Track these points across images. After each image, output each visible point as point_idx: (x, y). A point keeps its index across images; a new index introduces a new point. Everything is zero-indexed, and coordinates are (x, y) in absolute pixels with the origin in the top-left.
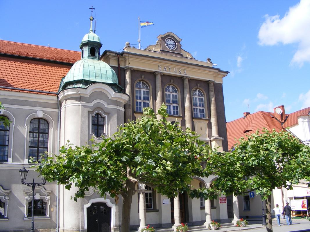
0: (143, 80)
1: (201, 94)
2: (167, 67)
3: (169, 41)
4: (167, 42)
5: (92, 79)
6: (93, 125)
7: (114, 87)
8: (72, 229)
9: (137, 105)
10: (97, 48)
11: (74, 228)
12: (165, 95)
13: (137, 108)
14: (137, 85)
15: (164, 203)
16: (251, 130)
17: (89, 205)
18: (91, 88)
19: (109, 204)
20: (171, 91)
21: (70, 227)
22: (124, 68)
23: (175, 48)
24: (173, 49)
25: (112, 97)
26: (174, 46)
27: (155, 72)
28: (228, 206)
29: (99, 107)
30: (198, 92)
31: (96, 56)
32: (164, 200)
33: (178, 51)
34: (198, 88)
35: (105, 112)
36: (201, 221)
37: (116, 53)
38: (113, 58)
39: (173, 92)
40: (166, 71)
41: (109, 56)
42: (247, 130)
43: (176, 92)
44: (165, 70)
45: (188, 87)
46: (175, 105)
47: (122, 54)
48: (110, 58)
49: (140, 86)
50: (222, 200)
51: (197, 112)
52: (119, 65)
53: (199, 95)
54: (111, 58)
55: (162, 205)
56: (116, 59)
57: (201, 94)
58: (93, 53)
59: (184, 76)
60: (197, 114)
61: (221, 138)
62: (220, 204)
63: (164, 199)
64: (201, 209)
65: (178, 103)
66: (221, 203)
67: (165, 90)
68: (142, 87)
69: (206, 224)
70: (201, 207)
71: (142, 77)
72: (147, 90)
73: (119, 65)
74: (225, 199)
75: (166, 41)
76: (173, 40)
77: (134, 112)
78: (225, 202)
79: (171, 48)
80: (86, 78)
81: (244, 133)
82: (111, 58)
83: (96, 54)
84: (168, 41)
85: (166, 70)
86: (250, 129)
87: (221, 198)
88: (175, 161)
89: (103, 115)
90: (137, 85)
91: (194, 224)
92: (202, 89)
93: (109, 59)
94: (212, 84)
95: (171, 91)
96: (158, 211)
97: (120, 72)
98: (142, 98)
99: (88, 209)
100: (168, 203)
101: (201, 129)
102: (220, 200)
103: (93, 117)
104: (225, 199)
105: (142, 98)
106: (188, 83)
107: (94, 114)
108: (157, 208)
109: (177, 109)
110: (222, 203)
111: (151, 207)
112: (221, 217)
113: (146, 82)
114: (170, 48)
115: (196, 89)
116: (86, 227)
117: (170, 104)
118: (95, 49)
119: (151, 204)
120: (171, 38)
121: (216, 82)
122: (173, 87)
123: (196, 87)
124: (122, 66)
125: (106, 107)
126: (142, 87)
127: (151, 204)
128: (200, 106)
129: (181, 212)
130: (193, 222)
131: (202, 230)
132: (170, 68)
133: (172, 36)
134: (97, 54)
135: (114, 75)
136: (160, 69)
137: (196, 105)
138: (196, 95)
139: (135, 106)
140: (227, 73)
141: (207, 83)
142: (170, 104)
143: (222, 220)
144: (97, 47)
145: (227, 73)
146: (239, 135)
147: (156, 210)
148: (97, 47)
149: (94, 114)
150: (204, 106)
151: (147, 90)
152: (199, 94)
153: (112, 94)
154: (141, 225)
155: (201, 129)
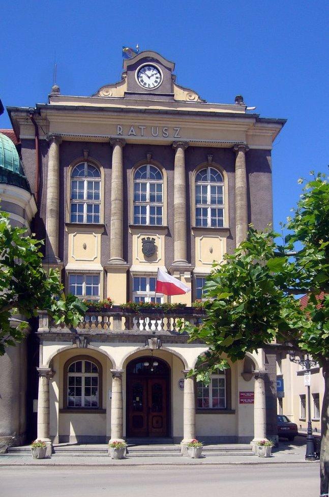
0: (87, 161)
2: (133, 126)
26: (156, 82)
37: (27, 111)
38: (26, 123)
44: (130, 133)
46: (156, 204)
47: (39, 111)
48: (20, 123)
49: (83, 172)
66: (241, 402)
69: (254, 444)
71: (83, 155)
79: (149, 85)
82: (23, 123)
85: (134, 133)
87: (243, 392)
88: (295, 330)
92: (218, 166)
102: (241, 396)
110: (245, 403)
112: (239, 432)
113: (93, 163)
114: (147, 86)
117: (144, 204)
121: (251, 147)
123: (205, 163)
124: (24, 135)
126: (86, 173)
131: (158, 456)
132: (142, 127)
136: (121, 132)
140: (282, 123)
145: (282, 123)
147: (231, 410)
154: (184, 436)
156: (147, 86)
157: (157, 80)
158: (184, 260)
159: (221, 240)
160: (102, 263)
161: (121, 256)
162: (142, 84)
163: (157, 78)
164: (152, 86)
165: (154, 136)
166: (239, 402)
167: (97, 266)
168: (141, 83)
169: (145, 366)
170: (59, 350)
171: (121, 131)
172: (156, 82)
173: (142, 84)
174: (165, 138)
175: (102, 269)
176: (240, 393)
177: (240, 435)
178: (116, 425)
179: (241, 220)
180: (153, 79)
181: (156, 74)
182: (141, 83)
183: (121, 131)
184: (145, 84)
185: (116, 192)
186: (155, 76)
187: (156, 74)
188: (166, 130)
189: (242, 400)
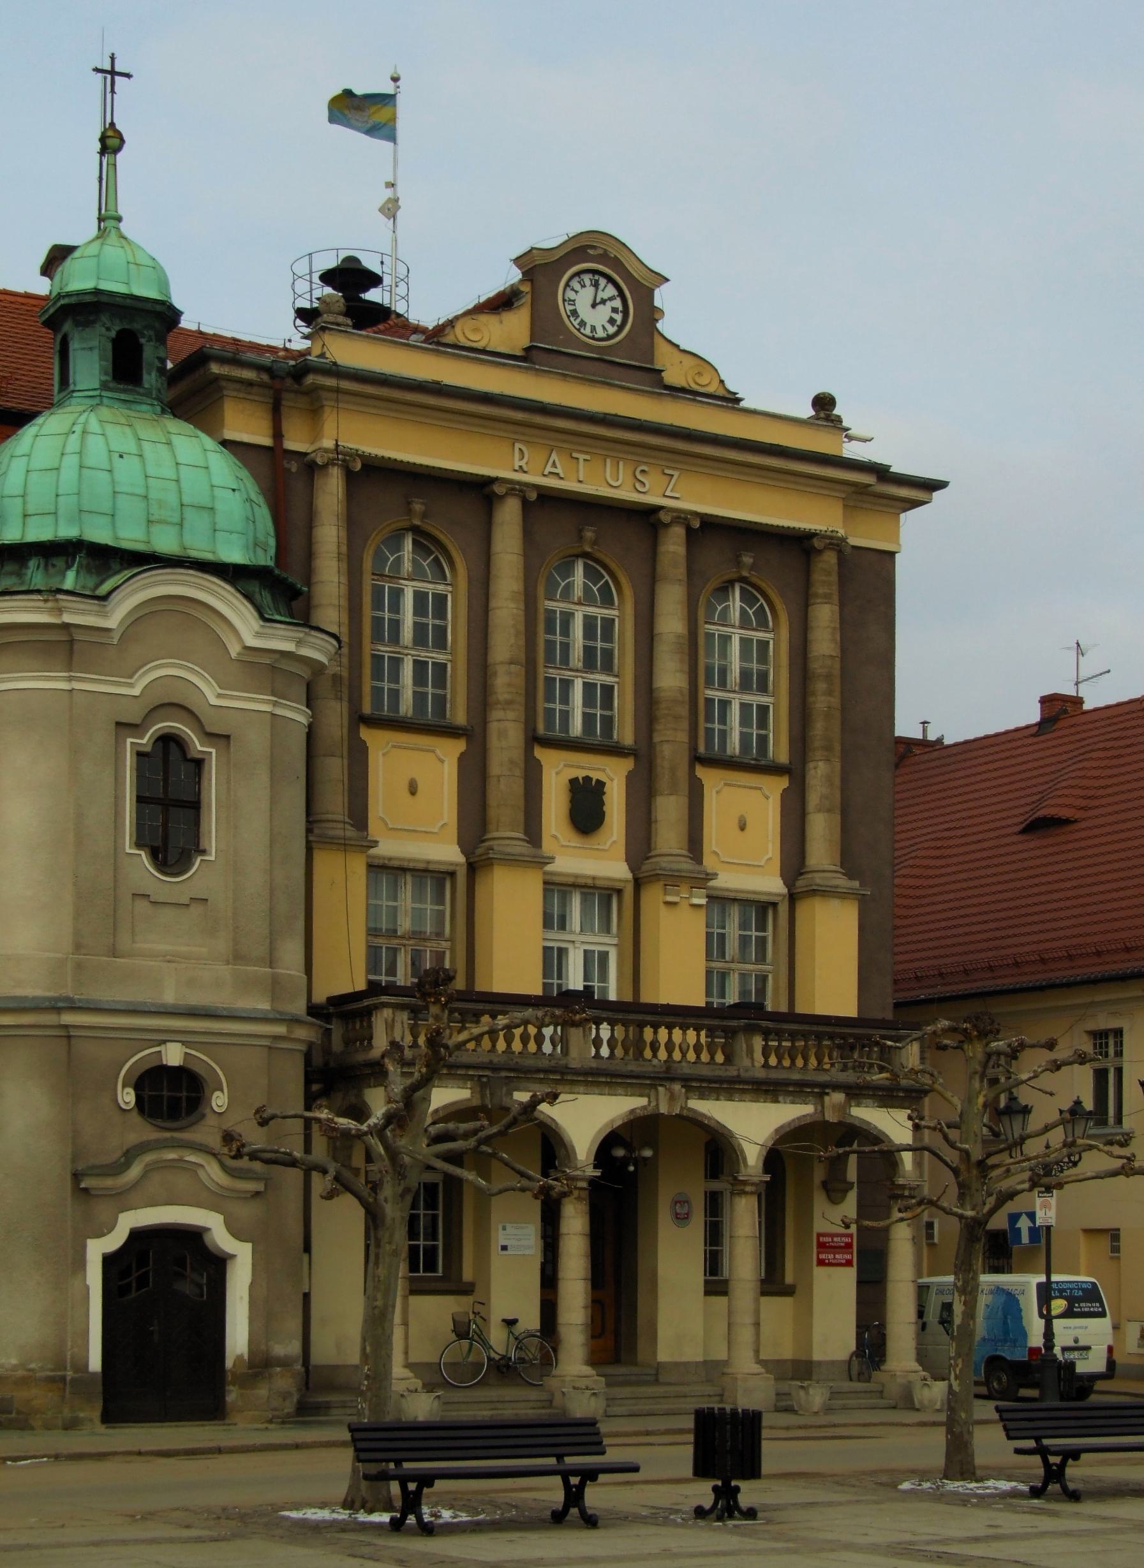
1: (760, 613)
3: (583, 286)
4: (570, 294)
5: (130, 537)
6: (140, 800)
7: (254, 587)
8: (25, 1373)
9: (377, 674)
10: (150, 340)
11: (33, 1366)
12: (541, 617)
13: (377, 692)
14: (380, 558)
15: (504, 1248)
16: (1067, 822)
17: (114, 1241)
18: (135, 594)
19: (221, 1238)
20: (578, 592)
21: (14, 1361)
22: (306, 454)
23: (621, 328)
24: (609, 337)
25: (246, 648)
26: (612, 321)
27: (489, 481)
28: (860, 1283)
29: (166, 701)
30: (738, 603)
31: (146, 386)
32: (504, 1229)
33: (636, 353)
34: (743, 580)
35: (209, 729)
36: (705, 1362)
39: (588, 598)
40: (557, 474)
41: (223, 383)
42: (1041, 813)
43: (607, 601)
44: (549, 469)
45: (681, 571)
46: (600, 678)
48: (225, 393)
49: (398, 562)
50: (828, 1251)
51: (723, 720)
52: (278, 435)
53: (745, 623)
54: (235, 394)
55: (497, 1260)
56: (261, 399)
57: (760, 613)
58: (125, 370)
59: (661, 508)
60: (723, 734)
61: (856, 884)
62: (819, 1272)
63: (508, 1226)
64: (708, 1293)
65: (616, 668)
66: (821, 1263)
67: (541, 591)
68: (407, 566)
70: (706, 1282)
71: (409, 512)
72: (441, 588)
73: (278, 435)
74: (849, 1246)
75: (567, 285)
76: (610, 280)
77: (360, 720)
78: (849, 1263)
79: (593, 328)
80: (99, 534)
81: (1024, 831)
83: (145, 377)
84: (577, 286)
85: (559, 470)
86: (1065, 813)
89: (198, 746)
90: (380, 558)
91: (661, 1379)
93: (222, 397)
94: (830, 559)
95: (578, 592)
96: (466, 1290)
97: (282, 479)
98: (407, 633)
99: (108, 1261)
100: (529, 1247)
101: (413, 790)
102: (822, 1246)
103: (140, 754)
104: (849, 1246)
105: (407, 633)
106: (681, 550)
107: (145, 740)
108: (468, 1274)
109: (608, 703)
111: (431, 1266)
114: (588, 331)
115: (731, 583)
116: (95, 1362)
117: (567, 674)
118: (143, 341)
119: (434, 1248)
120: (601, 267)
121: (853, 541)
122: (589, 573)
125: (214, 701)
127: (435, 1248)
128: (745, 683)
129: (593, 1301)
130: (659, 1367)
133: (604, 258)
134: (150, 374)
135: (256, 508)
136: (523, 463)
137: (723, 684)
138: (724, 620)
139: (367, 684)
141: (799, 545)
142: (567, 674)
143: (820, 1363)
144: (151, 333)
146: (1095, 889)
148: (151, 333)
149: (200, 748)
150: (771, 687)
151: (441, 588)
152: (743, 612)
153: (243, 623)
155: (413, 790)
156: (588, 331)
157: (615, 316)
158: (833, 868)
159: (767, 798)
160: (461, 843)
161: (686, 847)
162: (576, 323)
163: (614, 310)
164: (600, 333)
165: (611, 486)
166: (815, 1262)
167: (771, 884)
168: (572, 319)
169: (616, 1158)
170: (632, 1111)
171: (525, 460)
172: (612, 321)
173: (576, 323)
174: (613, 490)
175: (461, 859)
176: (819, 1235)
177: (817, 1356)
178: (580, 1328)
179: (828, 748)
180: (604, 312)
181: (611, 299)
182: (572, 319)
183: (525, 460)
184: (583, 324)
185: (512, 641)
186: (609, 304)
187: (611, 299)
188: (643, 471)
189: (822, 1256)
